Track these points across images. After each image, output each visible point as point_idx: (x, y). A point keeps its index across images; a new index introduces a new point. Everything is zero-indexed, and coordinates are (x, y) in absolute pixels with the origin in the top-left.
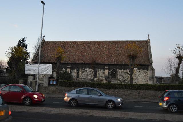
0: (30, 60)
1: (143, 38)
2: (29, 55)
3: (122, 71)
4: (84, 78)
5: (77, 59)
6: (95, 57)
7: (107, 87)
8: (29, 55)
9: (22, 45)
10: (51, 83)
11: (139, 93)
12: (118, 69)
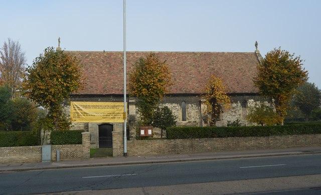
10: (142, 132)
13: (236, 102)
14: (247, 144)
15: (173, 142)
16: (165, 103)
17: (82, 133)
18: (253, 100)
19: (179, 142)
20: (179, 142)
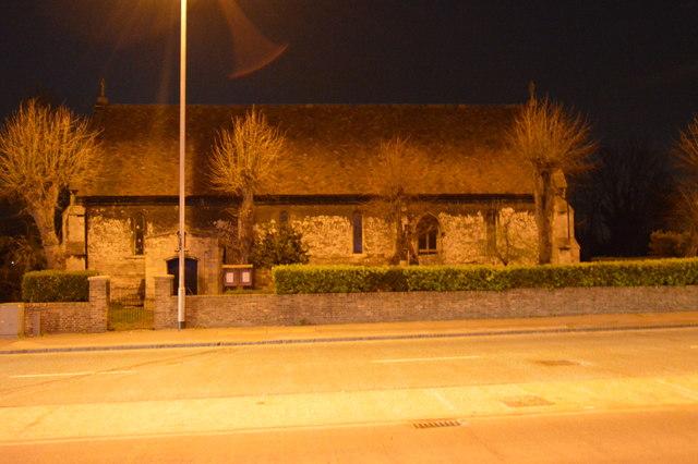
3: (458, 219)
10: (230, 278)
12: (441, 214)
13: (474, 214)
15: (288, 300)
18: (511, 210)
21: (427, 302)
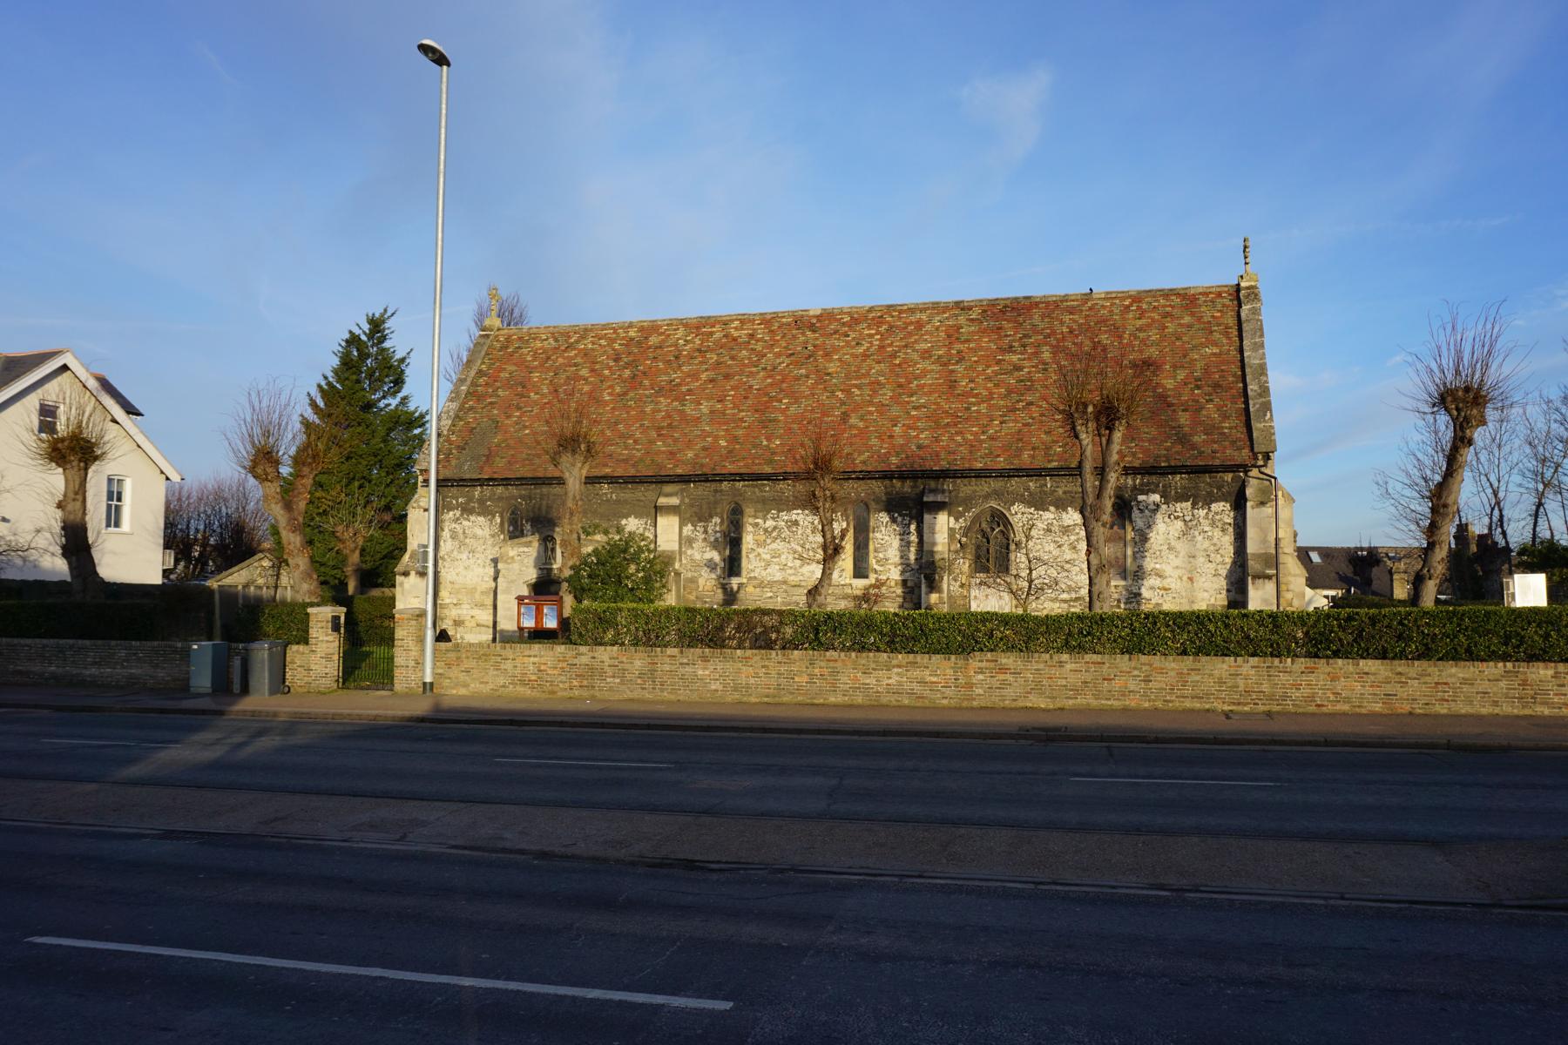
0: (430, 460)
1: (1208, 271)
2: (417, 431)
3: (1049, 515)
4: (778, 576)
5: (723, 443)
6: (851, 427)
7: (915, 628)
8: (417, 431)
9: (367, 365)
11: (1147, 681)
12: (1014, 508)
14: (871, 681)
16: (789, 510)
17: (309, 610)
19: (605, 658)
20: (605, 658)
21: (817, 671)
